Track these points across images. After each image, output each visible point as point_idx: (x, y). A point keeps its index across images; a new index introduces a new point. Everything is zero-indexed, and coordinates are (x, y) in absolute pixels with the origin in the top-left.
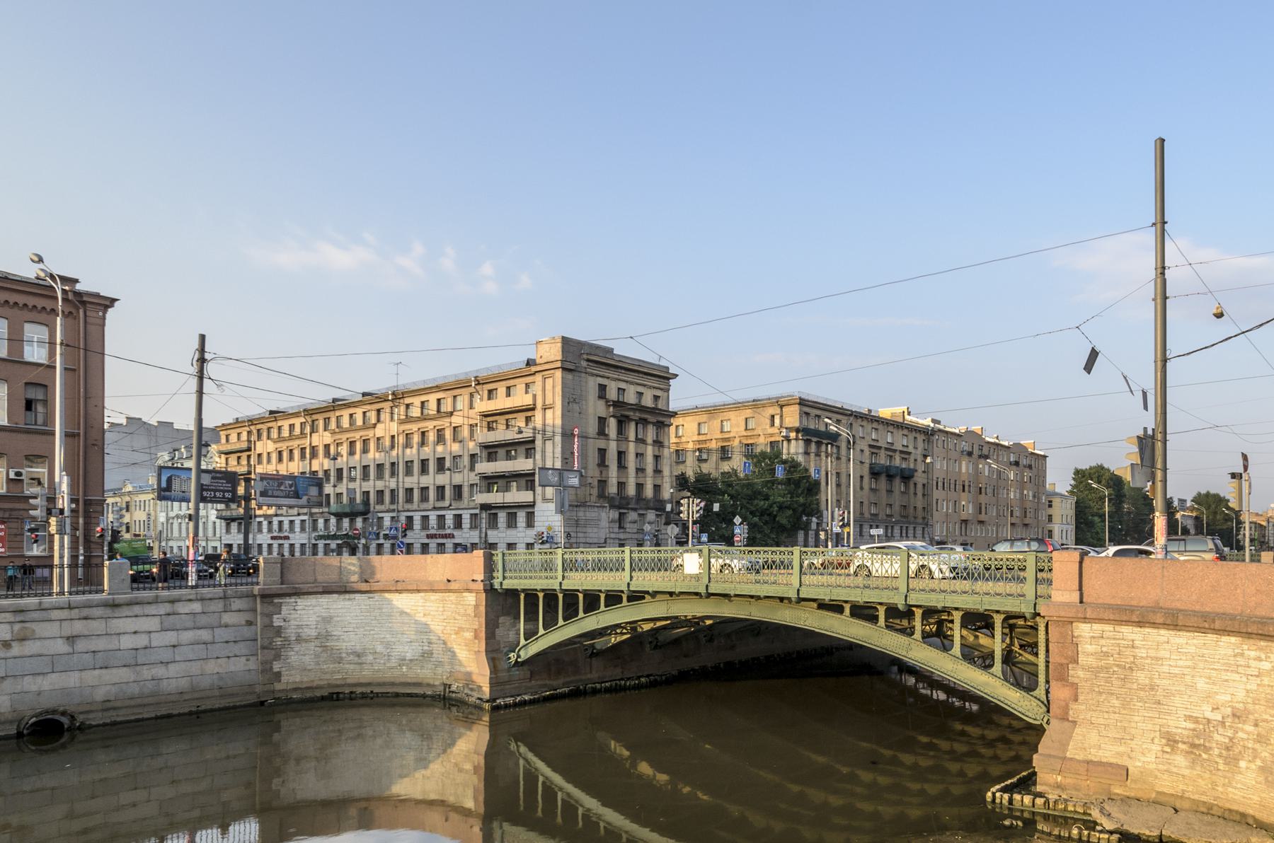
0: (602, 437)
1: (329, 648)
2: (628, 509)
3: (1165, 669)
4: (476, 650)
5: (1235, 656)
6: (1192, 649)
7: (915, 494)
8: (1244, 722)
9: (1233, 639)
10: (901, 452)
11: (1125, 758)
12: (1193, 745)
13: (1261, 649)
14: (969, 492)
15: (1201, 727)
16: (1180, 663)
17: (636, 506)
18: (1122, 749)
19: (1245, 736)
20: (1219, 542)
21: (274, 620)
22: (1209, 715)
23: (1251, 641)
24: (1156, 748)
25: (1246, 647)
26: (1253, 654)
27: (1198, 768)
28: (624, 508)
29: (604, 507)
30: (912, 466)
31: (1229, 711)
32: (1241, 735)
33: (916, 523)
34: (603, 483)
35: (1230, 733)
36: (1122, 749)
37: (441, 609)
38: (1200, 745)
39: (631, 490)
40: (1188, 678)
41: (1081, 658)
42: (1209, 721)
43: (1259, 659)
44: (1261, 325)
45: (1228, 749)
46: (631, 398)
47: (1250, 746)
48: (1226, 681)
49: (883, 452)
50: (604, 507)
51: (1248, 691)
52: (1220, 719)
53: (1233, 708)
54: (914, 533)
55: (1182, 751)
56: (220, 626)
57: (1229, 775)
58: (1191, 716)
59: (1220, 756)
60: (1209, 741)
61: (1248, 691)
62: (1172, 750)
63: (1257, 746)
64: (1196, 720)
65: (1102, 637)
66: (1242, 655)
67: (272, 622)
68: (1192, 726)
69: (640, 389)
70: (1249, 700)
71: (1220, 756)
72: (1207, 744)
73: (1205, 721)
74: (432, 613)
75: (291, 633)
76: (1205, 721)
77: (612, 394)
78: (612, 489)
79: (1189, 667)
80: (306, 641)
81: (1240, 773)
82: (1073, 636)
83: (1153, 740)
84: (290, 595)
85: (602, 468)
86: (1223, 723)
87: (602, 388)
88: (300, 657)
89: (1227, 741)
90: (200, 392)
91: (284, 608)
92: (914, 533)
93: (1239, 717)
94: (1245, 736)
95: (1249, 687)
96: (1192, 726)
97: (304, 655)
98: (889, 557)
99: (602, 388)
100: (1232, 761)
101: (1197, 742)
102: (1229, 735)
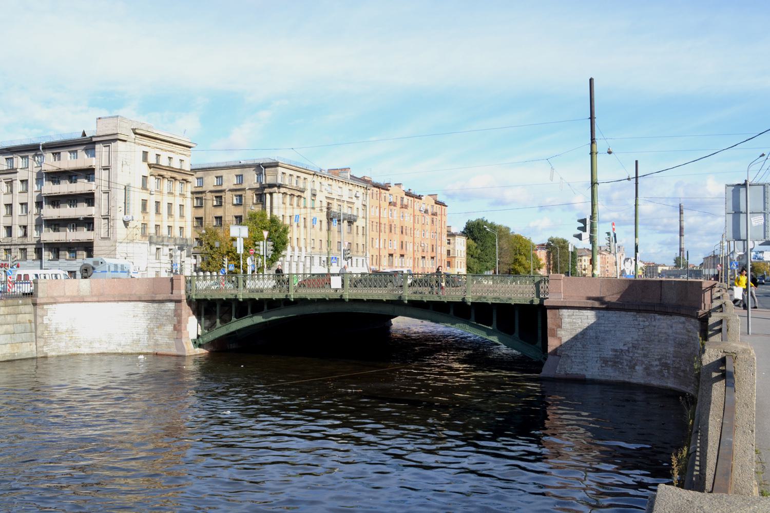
0: (144, 191)
1: (74, 338)
2: (163, 245)
3: (603, 328)
4: (175, 337)
5: (633, 320)
6: (614, 319)
7: (357, 234)
8: (638, 349)
9: (632, 313)
10: (338, 200)
11: (584, 371)
12: (615, 362)
13: (644, 317)
14: (385, 232)
15: (619, 353)
16: (610, 325)
17: (168, 243)
18: (583, 367)
19: (638, 355)
20: (667, 268)
21: (44, 320)
22: (622, 348)
23: (640, 314)
24: (598, 365)
25: (638, 316)
26: (641, 319)
27: (617, 372)
28: (159, 245)
29: (145, 243)
30: (355, 214)
31: (631, 345)
32: (636, 355)
33: (358, 256)
34: (144, 225)
35: (631, 355)
36: (583, 367)
37: (146, 313)
38: (618, 361)
39: (164, 231)
40: (613, 332)
41: (563, 325)
42: (622, 350)
43: (644, 321)
44: (643, 176)
45: (630, 362)
46: (164, 162)
47: (640, 359)
48: (630, 332)
49: (345, 204)
50: (145, 243)
51: (638, 335)
52: (627, 349)
53: (633, 344)
54: (357, 264)
55: (610, 365)
56: (17, 323)
57: (631, 373)
58: (614, 349)
59: (627, 365)
60: (622, 360)
61: (638, 335)
62: (606, 365)
63: (643, 359)
64: (616, 351)
65: (573, 315)
66: (636, 320)
67: (43, 321)
68: (614, 353)
69: (171, 155)
70: (640, 339)
71: (627, 365)
72: (621, 361)
73: (620, 351)
74: (139, 315)
75: (52, 328)
76: (620, 351)
77: (152, 160)
78: (151, 230)
79: (613, 327)
80: (61, 333)
81: (636, 372)
82: (559, 315)
83: (597, 361)
84: (52, 303)
85: (144, 214)
86: (628, 351)
87: (145, 153)
88: (58, 343)
89: (630, 358)
90: (125, 193)
91: (49, 312)
92: (357, 264)
93: (635, 347)
94: (638, 355)
95: (639, 334)
96: (614, 353)
97: (60, 342)
98: (266, 286)
99: (145, 153)
100: (632, 367)
101: (617, 360)
102: (631, 355)
